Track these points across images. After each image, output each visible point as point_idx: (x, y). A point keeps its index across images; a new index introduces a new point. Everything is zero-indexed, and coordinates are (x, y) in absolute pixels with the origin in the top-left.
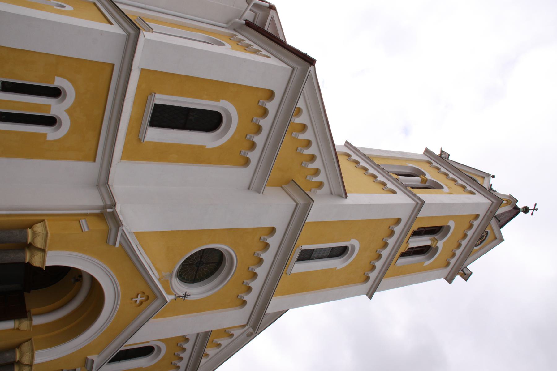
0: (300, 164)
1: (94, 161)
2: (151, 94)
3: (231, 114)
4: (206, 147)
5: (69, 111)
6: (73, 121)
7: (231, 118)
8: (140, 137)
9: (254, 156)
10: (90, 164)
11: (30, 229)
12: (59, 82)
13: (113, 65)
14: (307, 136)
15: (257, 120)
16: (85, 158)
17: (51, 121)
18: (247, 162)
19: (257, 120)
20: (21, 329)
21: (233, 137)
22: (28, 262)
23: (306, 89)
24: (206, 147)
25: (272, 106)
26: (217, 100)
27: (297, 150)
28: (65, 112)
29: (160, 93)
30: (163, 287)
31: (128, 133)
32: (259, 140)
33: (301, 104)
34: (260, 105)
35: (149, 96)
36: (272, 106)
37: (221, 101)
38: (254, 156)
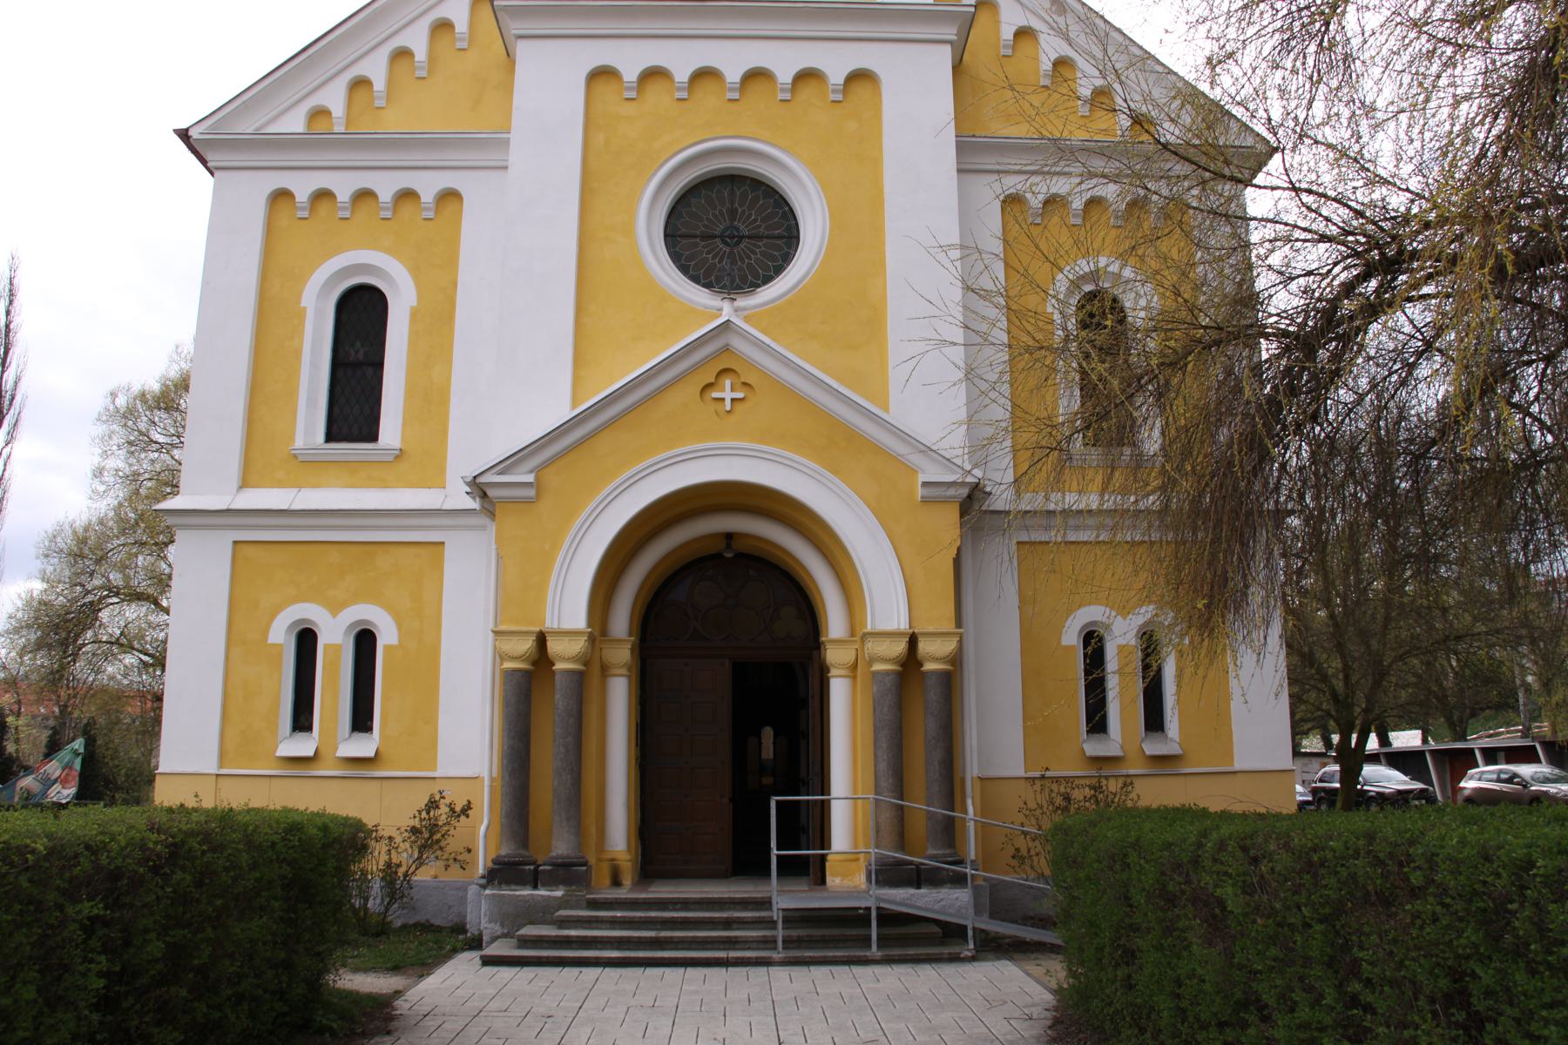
0: (462, 53)
1: (443, 543)
2: (295, 456)
3: (339, 267)
4: (415, 304)
5: (335, 608)
6: (356, 598)
7: (345, 268)
8: (391, 458)
9: (428, 186)
10: (448, 551)
11: (554, 665)
12: (1071, 637)
13: (235, 543)
14: (376, 69)
15: (834, 91)
16: (438, 565)
17: (365, 641)
18: (450, 196)
19: (834, 91)
20: (853, 659)
21: (387, 251)
22: (901, 666)
23: (246, 127)
24: (415, 304)
25: (302, 186)
26: (301, 314)
27: (424, 78)
28: (339, 616)
29: (292, 438)
30: (709, 322)
31: (384, 484)
32: (386, 186)
33: (295, 123)
34: (790, 95)
35: (300, 459)
36: (302, 186)
37: (303, 304)
38: (428, 186)
